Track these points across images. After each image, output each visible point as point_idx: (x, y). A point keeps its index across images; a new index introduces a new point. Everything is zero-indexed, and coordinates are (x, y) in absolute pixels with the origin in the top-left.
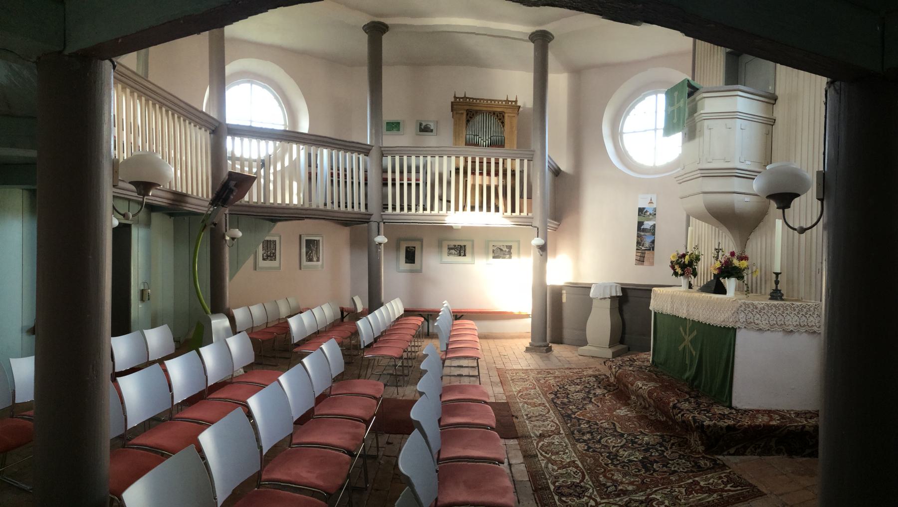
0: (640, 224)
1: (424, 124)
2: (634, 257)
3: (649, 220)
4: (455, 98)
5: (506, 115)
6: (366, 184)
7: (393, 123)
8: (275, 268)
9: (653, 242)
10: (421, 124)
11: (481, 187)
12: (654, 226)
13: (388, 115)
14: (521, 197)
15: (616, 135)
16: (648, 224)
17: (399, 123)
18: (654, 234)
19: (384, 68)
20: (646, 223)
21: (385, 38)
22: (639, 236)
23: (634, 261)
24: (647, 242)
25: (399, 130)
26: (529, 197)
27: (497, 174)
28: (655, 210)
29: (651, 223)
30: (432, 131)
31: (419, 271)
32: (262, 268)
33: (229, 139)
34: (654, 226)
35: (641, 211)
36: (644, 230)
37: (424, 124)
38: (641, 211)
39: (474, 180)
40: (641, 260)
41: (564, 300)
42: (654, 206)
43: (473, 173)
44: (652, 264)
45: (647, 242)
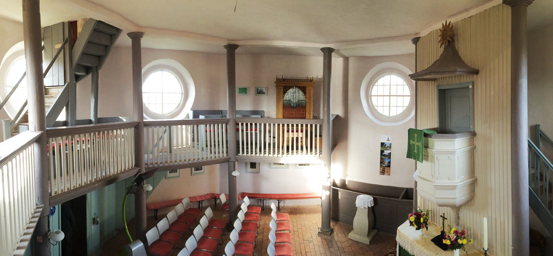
0: (382, 152)
1: (259, 89)
2: (379, 170)
3: (387, 150)
4: (277, 79)
5: (307, 89)
6: (227, 144)
7: (243, 89)
8: (176, 177)
9: (390, 162)
10: (258, 89)
11: (293, 138)
12: (390, 153)
13: (239, 84)
14: (316, 136)
15: (368, 96)
16: (386, 152)
17: (246, 89)
18: (390, 158)
19: (236, 56)
20: (385, 151)
21: (237, 51)
22: (381, 159)
23: (379, 173)
24: (386, 162)
25: (246, 93)
26: (320, 136)
27: (302, 131)
28: (391, 144)
29: (389, 152)
30: (264, 93)
31: (258, 172)
32: (170, 178)
33: (145, 129)
34: (390, 153)
35: (382, 144)
36: (385, 155)
37: (259, 89)
38: (382, 144)
39: (288, 135)
40: (383, 172)
41: (340, 197)
42: (390, 142)
43: (288, 131)
44: (389, 175)
45: (386, 162)
